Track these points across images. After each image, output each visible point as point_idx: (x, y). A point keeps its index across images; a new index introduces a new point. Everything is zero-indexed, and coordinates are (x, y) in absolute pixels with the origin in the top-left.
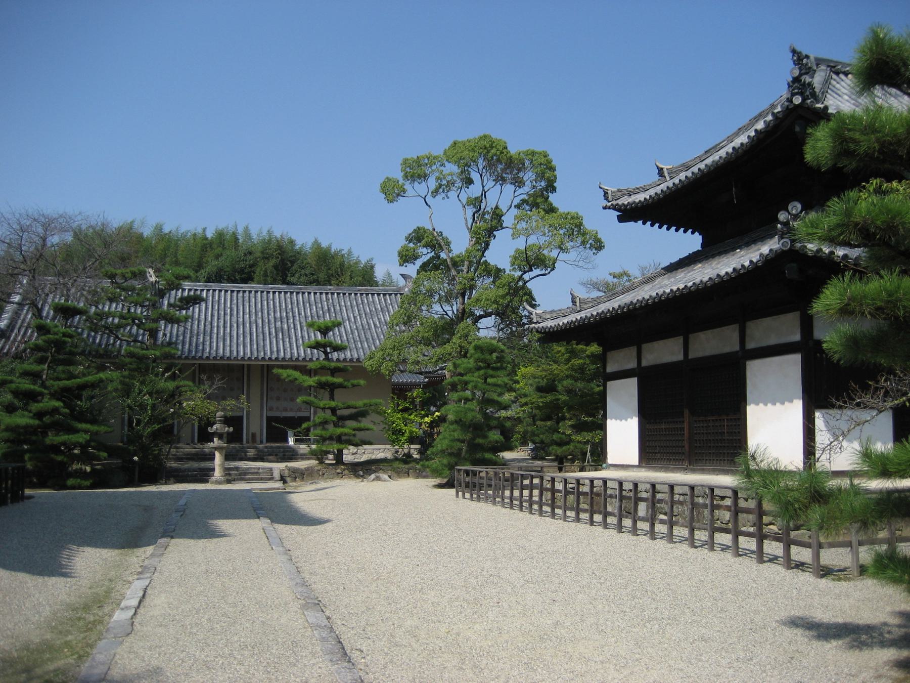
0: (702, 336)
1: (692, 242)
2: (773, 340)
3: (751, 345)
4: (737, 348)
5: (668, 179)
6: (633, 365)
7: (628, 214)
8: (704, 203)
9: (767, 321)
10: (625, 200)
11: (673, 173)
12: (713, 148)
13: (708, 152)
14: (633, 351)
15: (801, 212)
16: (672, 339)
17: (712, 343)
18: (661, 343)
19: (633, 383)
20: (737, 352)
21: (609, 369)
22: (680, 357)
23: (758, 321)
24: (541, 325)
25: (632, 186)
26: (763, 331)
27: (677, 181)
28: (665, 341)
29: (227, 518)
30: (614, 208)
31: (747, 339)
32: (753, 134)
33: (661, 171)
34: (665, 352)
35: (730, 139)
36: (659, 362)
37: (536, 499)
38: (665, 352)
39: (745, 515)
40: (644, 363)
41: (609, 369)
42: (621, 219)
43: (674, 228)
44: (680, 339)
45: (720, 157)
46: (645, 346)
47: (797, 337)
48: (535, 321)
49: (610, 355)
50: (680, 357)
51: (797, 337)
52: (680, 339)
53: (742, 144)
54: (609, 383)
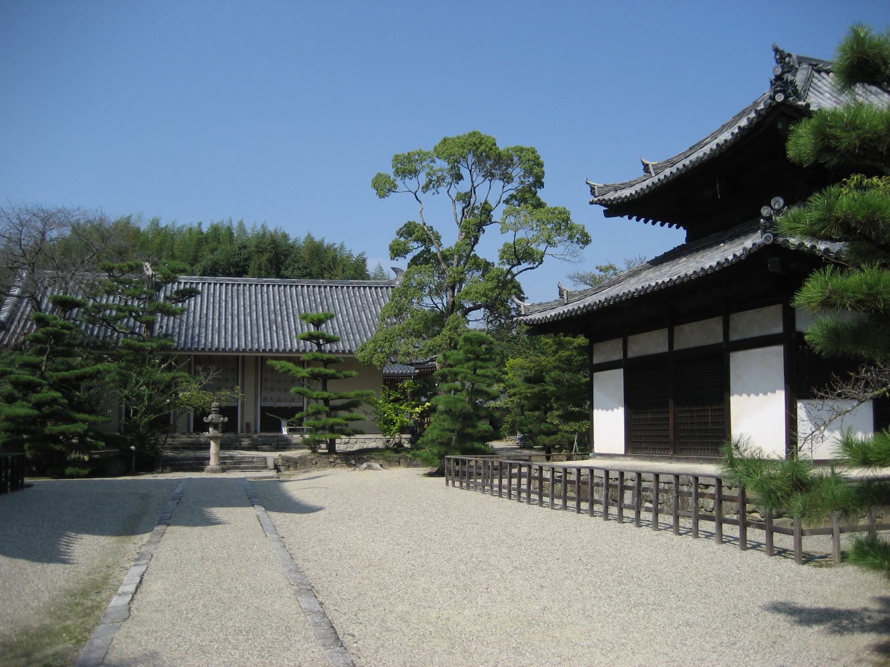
0: (687, 328)
1: (677, 236)
2: (756, 333)
3: (734, 337)
4: (720, 340)
5: (653, 174)
6: (619, 356)
7: (614, 209)
8: (689, 198)
9: (750, 314)
10: (611, 196)
11: (658, 169)
12: (697, 145)
13: (693, 149)
14: (619, 342)
15: (783, 207)
16: (657, 331)
17: (697, 335)
18: (647, 334)
19: (619, 374)
20: (721, 344)
21: (596, 361)
22: (666, 349)
23: (741, 313)
24: (529, 317)
25: (618, 182)
26: (747, 323)
27: (662, 177)
28: (651, 333)
29: (222, 506)
30: (601, 203)
31: (731, 331)
32: (736, 131)
33: (646, 167)
34: (650, 344)
35: (714, 136)
36: (644, 353)
37: (524, 487)
38: (650, 344)
39: (728, 503)
40: (630, 355)
41: (596, 361)
42: (607, 214)
43: (659, 223)
44: (665, 331)
45: (705, 154)
46: (631, 338)
47: (779, 329)
48: (523, 313)
49: (597, 346)
50: (666, 349)
51: (779, 329)
52: (665, 331)
53: (726, 141)
54: (595, 374)
